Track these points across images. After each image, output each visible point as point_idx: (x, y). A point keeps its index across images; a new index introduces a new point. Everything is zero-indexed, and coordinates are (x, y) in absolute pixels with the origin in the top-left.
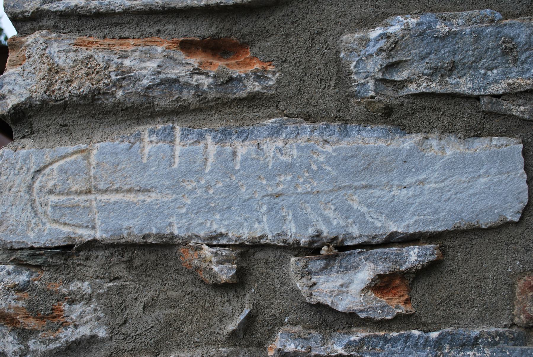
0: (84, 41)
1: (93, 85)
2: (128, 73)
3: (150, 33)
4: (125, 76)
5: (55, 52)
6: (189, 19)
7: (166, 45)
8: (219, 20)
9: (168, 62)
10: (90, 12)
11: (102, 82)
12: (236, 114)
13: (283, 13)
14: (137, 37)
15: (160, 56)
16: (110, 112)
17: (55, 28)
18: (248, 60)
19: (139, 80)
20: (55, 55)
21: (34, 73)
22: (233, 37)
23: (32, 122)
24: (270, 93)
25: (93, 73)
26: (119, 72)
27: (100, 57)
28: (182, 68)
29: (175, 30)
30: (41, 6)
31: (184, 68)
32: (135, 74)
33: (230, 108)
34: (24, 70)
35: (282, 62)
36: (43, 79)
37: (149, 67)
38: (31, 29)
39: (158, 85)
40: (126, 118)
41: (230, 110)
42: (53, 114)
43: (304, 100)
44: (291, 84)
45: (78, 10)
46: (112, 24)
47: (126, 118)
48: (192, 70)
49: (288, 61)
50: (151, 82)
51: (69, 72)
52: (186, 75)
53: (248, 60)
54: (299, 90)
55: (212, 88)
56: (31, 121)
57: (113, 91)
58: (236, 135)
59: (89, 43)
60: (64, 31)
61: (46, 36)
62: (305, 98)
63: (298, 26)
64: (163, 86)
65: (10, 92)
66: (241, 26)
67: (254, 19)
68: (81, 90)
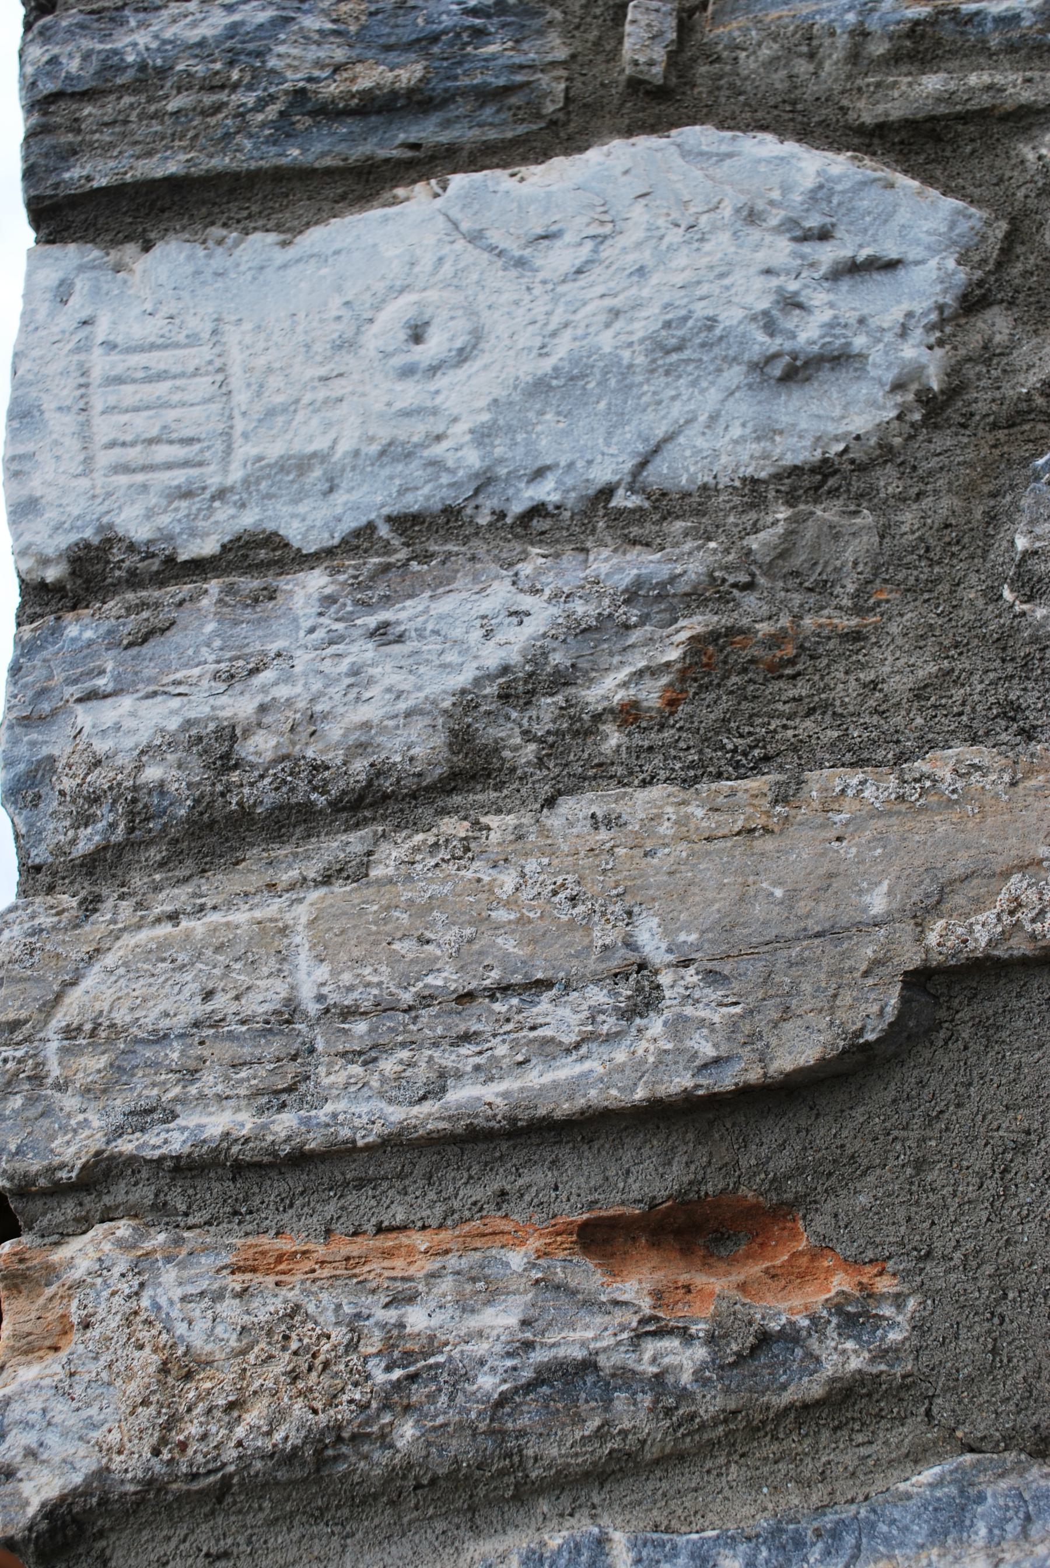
0: (263, 1253)
1: (315, 1412)
2: (426, 1356)
3: (475, 1204)
4: (417, 1368)
5: (171, 1303)
6: (596, 1146)
7: (534, 1243)
8: (690, 1136)
9: (551, 1301)
10: (275, 1154)
11: (345, 1398)
12: (796, 1459)
13: (891, 1094)
14: (435, 1224)
15: (523, 1284)
16: (375, 1497)
17: (160, 1212)
18: (804, 1261)
19: (467, 1378)
20: (175, 1314)
21: (109, 1384)
22: (743, 1190)
23: (108, 1552)
24: (898, 1371)
25: (310, 1369)
26: (396, 1354)
27: (326, 1307)
28: (599, 1320)
29: (556, 1189)
30: (108, 1143)
31: (607, 1318)
32: (450, 1359)
33: (775, 1438)
34: (72, 1375)
35: (919, 1259)
36: (145, 1403)
37: (492, 1328)
38: (77, 1220)
39: (530, 1387)
40: (431, 1511)
41: (775, 1447)
42: (181, 1519)
43: (1015, 1385)
44: (963, 1332)
45: (235, 1149)
46: (346, 1184)
47: (431, 1511)
48: (634, 1324)
49: (938, 1253)
50: (505, 1381)
51: (229, 1374)
52: (619, 1343)
53: (804, 1261)
54: (994, 1351)
55: (710, 1379)
56: (103, 1550)
57: (382, 1428)
58: (820, 1545)
59: (279, 1259)
60: (191, 1221)
61: (134, 1247)
62: (1019, 1377)
63: (947, 1129)
64: (545, 1390)
65: (31, 1454)
66: (764, 1151)
67: (803, 1124)
68: (278, 1436)
